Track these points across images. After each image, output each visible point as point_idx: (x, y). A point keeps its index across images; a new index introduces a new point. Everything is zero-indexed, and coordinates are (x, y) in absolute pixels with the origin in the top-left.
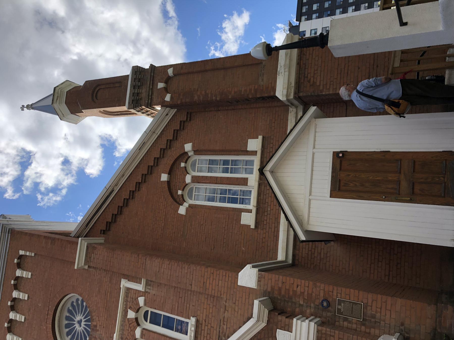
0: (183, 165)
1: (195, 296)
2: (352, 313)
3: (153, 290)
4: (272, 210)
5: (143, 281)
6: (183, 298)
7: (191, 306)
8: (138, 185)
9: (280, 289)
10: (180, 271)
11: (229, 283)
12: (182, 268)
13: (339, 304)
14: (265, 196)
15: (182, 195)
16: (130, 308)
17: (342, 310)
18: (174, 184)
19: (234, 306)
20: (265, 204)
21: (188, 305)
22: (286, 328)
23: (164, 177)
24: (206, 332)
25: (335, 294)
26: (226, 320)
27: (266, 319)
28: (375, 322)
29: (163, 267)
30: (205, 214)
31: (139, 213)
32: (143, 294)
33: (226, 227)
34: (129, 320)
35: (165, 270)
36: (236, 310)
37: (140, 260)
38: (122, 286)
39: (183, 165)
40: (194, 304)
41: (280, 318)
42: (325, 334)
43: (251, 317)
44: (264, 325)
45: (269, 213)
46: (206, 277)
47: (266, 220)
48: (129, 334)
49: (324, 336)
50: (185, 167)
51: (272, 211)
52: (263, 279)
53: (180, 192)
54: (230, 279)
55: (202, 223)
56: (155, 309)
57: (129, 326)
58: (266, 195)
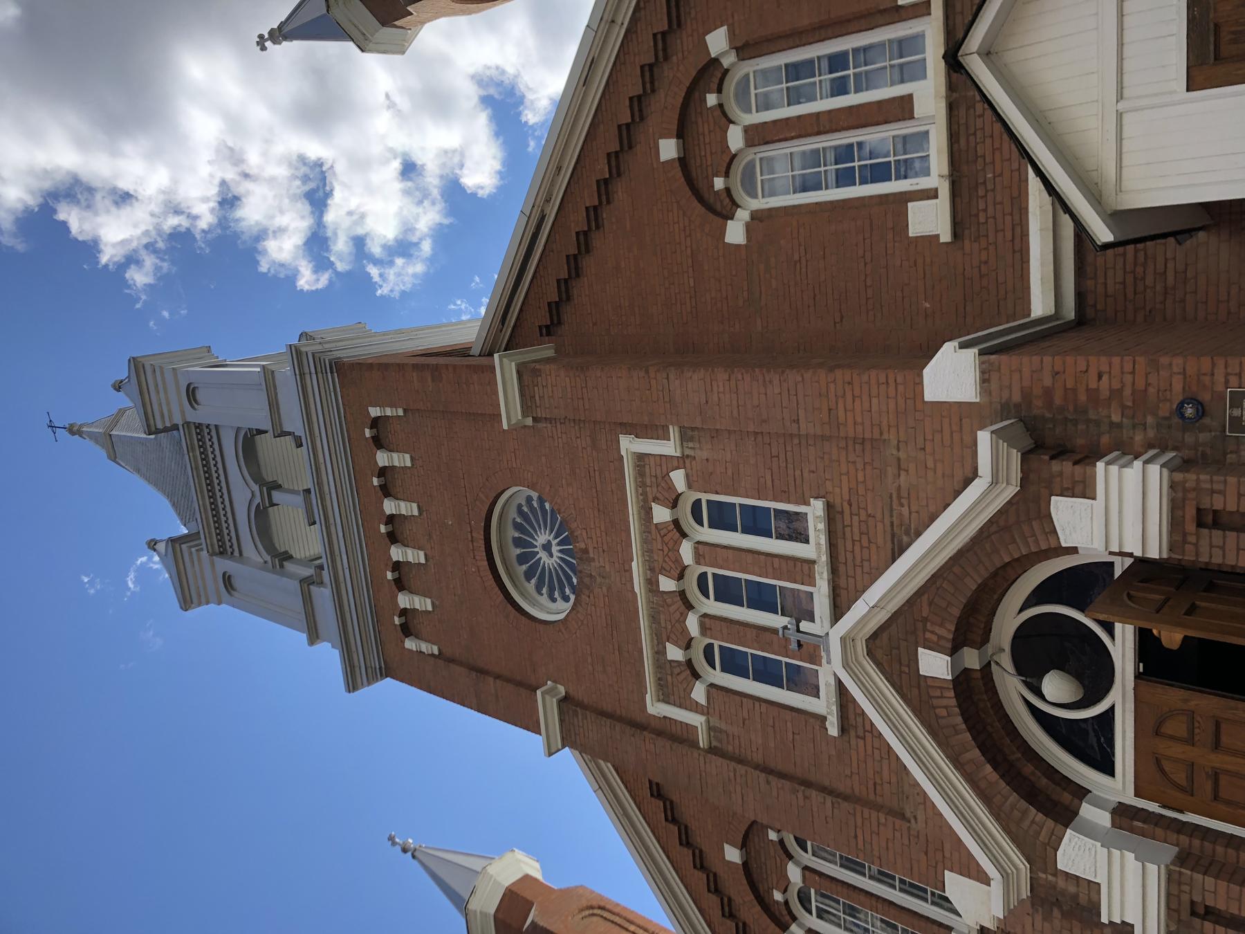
4: (1001, 175)
5: (673, 431)
6: (782, 456)
7: (806, 474)
8: (604, 186)
11: (901, 401)
12: (765, 386)
14: (972, 138)
20: (976, 161)
21: (798, 473)
22: (1078, 489)
23: (668, 149)
24: (856, 530)
33: (868, 255)
36: (930, 464)
37: (653, 382)
39: (712, 99)
40: (813, 468)
41: (1056, 466)
42: (1194, 489)
44: (1010, 491)
45: (990, 186)
46: (832, 395)
47: (985, 210)
49: (1192, 495)
54: (901, 388)
55: (796, 257)
56: (717, 493)
57: (663, 541)
58: (975, 134)
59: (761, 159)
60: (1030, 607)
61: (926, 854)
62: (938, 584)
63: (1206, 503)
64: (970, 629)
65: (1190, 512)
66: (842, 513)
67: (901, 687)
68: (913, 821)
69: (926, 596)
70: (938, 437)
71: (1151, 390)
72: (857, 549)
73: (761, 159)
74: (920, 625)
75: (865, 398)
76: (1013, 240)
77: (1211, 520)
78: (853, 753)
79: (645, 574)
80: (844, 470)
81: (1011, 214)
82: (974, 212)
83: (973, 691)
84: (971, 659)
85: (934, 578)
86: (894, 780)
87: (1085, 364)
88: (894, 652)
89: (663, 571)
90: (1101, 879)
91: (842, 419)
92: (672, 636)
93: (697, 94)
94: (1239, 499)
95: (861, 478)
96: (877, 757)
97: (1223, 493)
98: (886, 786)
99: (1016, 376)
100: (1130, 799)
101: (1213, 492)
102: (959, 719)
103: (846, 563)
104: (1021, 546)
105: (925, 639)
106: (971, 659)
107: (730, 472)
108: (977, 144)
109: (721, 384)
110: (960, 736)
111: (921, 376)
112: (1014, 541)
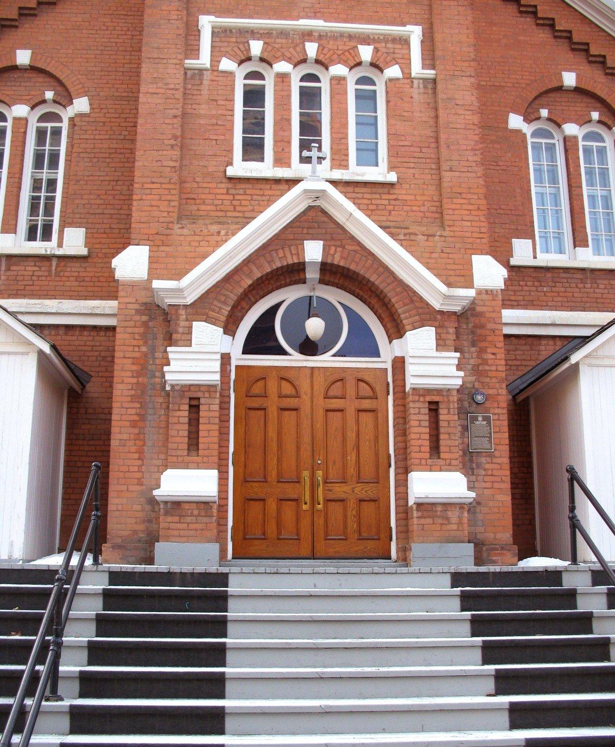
0: (595, 115)
1: (429, 177)
2: (475, 437)
3: (419, 93)
4: (545, 295)
5: (430, 73)
6: (421, 155)
7: (412, 171)
9: (482, 327)
10: (469, 148)
11: (470, 240)
12: (472, 150)
13: (485, 419)
14: (566, 281)
15: (538, 118)
16: (376, 50)
17: (478, 423)
18: (558, 100)
19: (439, 250)
21: (412, 165)
22: (441, 342)
23: (569, 79)
24: (379, 202)
25: (497, 411)
26: (412, 237)
27: (445, 308)
28: (472, 469)
29: (467, 113)
30: (517, 169)
31: (494, 29)
32: (407, 75)
33: (502, 212)
34: (355, 49)
35: (462, 117)
36: (434, 255)
37: (467, 64)
38: (409, 28)
39: (595, 115)
40: (417, 176)
42: (449, 400)
43: (306, 191)
44: (437, 305)
45: (539, 289)
46: (470, 196)
47: (526, 285)
48: (331, 52)
49: (446, 399)
50: (590, 121)
51: (543, 294)
52: (490, 297)
53: (544, 113)
54: (478, 241)
55: (500, 163)
56: (388, 102)
57: (345, 51)
58: (567, 282)
59: (554, 144)
60: (345, 311)
61: (157, 234)
62: (370, 257)
63: (441, 406)
64: (331, 273)
65: (436, 399)
66: (389, 193)
67: (292, 227)
68: (180, 226)
69: (359, 249)
70: (450, 261)
71: (488, 380)
72: (366, 201)
73: (554, 144)
74: (339, 243)
75: (470, 218)
76: (509, 300)
77: (434, 409)
78: (214, 185)
79: (316, 31)
80: (418, 198)
81: (523, 300)
82: (526, 279)
83: (294, 273)
84: (312, 274)
85: (371, 254)
86: (201, 213)
87: (500, 346)
88: (316, 225)
89: (321, 49)
90: (194, 348)
91: (455, 201)
92: (270, 48)
93: (599, 105)
94: (447, 421)
95: (414, 208)
96: (216, 202)
97: (449, 413)
98: (195, 208)
99: (491, 309)
100: (234, 363)
101: (449, 409)
102: (279, 265)
103: (354, 192)
104: (403, 309)
105: (330, 246)
106: (312, 274)
107: (405, 114)
108: (562, 283)
109: (470, 117)
110: (267, 264)
111: (487, 254)
112: (405, 305)
